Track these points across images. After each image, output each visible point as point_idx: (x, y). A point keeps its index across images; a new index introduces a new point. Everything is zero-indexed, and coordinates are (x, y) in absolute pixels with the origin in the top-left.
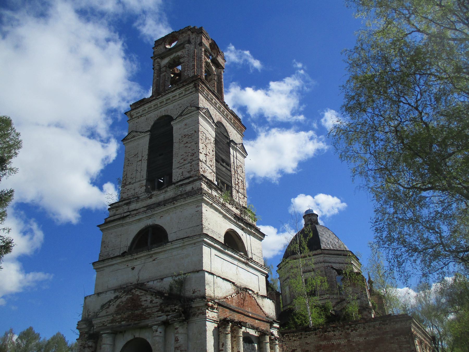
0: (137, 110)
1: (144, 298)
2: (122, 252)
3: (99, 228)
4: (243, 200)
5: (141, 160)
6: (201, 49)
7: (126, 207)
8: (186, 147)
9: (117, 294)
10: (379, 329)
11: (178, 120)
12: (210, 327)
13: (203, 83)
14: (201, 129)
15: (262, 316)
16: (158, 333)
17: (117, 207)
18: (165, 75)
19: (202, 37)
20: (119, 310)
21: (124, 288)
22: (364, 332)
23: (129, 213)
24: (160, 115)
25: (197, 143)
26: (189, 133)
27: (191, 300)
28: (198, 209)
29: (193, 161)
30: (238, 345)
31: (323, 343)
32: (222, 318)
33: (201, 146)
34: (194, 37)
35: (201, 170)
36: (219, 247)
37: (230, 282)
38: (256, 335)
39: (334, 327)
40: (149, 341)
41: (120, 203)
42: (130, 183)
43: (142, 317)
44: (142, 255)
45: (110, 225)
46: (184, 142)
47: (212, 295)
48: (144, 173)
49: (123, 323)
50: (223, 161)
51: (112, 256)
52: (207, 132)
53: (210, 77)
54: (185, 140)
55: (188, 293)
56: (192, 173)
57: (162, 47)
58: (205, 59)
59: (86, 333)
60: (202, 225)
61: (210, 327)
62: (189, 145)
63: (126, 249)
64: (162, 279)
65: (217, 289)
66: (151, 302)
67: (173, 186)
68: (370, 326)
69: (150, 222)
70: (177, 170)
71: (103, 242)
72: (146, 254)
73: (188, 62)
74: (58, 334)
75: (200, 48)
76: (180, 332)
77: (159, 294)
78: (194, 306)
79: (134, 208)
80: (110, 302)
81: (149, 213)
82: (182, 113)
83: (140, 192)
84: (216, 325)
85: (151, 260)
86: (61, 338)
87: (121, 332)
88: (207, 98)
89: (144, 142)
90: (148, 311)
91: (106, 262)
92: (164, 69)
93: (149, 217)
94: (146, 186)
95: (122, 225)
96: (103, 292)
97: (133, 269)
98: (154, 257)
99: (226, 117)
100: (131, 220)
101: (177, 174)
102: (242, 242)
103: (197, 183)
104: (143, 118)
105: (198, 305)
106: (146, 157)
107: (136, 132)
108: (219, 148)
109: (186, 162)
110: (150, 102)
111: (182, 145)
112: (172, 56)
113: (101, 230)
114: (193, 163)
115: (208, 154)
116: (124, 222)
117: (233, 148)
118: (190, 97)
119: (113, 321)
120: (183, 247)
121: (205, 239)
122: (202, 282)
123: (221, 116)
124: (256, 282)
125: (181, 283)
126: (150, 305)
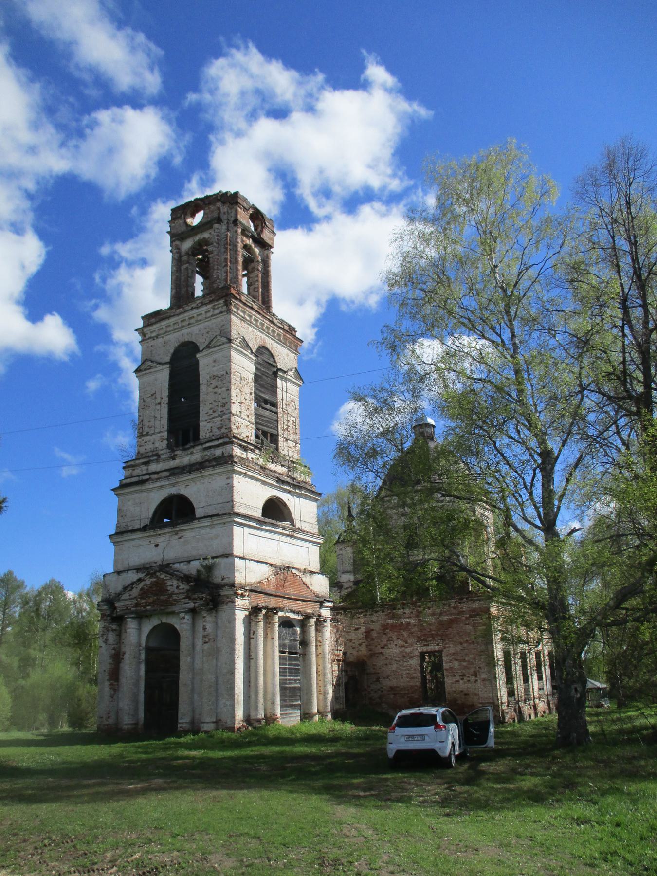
0: (151, 328)
1: (169, 583)
2: (142, 525)
3: (113, 492)
4: (294, 449)
5: (160, 404)
6: (236, 231)
7: (144, 467)
8: (216, 393)
9: (141, 575)
10: (454, 608)
11: (205, 352)
12: (240, 616)
13: (236, 298)
14: (234, 368)
15: (310, 596)
16: (185, 621)
17: (132, 466)
18: (187, 269)
19: (237, 210)
20: (144, 593)
21: (148, 568)
22: (438, 611)
23: (147, 477)
24: (182, 340)
25: (229, 390)
26: (220, 374)
27: (219, 587)
28: (229, 481)
29: (224, 414)
30: (273, 631)
31: (390, 622)
32: (255, 604)
33: (234, 392)
34: (225, 210)
35: (233, 427)
36: (254, 524)
37: (267, 563)
38: (300, 617)
39: (404, 604)
40: (177, 627)
41: (137, 462)
42: (147, 434)
43: (169, 603)
44: (166, 531)
45: (126, 490)
46: (213, 386)
47: (243, 581)
48: (165, 422)
49: (148, 608)
50: (266, 402)
51: (131, 528)
52: (243, 367)
53: (252, 265)
54: (215, 383)
55: (217, 580)
56: (223, 430)
57: (181, 222)
58: (243, 241)
59: (109, 615)
60: (233, 501)
61: (240, 616)
62: (219, 391)
63: (147, 522)
64: (189, 562)
65: (247, 573)
66: (178, 587)
67: (200, 447)
68: (444, 605)
69: (173, 491)
70: (205, 423)
71: (119, 510)
72: (170, 530)
73: (218, 255)
74: (52, 581)
75: (235, 228)
76: (207, 621)
77: (186, 578)
78: (222, 593)
79: (154, 470)
80: (132, 584)
81: (173, 480)
82: (210, 343)
83: (160, 448)
84: (247, 613)
85: (176, 537)
86: (57, 587)
87: (147, 616)
88: (243, 319)
89: (162, 376)
90: (175, 597)
91: (125, 535)
92: (185, 258)
93: (173, 485)
94: (168, 439)
95: (141, 491)
96: (124, 571)
97: (157, 546)
98: (180, 534)
99: (273, 336)
100: (151, 486)
101: (205, 429)
102: (288, 509)
103: (228, 447)
104: (160, 340)
105: (226, 593)
106: (166, 400)
107: (152, 362)
108: (260, 385)
109: (216, 414)
110: (168, 318)
111: (210, 389)
112: (197, 238)
113: (117, 495)
114: (224, 417)
115: (244, 401)
116: (143, 488)
117: (282, 378)
118: (219, 320)
119: (137, 605)
120: (212, 526)
121: (236, 519)
122: (232, 568)
123: (263, 336)
124: (304, 555)
125: (209, 569)
126: (176, 591)
